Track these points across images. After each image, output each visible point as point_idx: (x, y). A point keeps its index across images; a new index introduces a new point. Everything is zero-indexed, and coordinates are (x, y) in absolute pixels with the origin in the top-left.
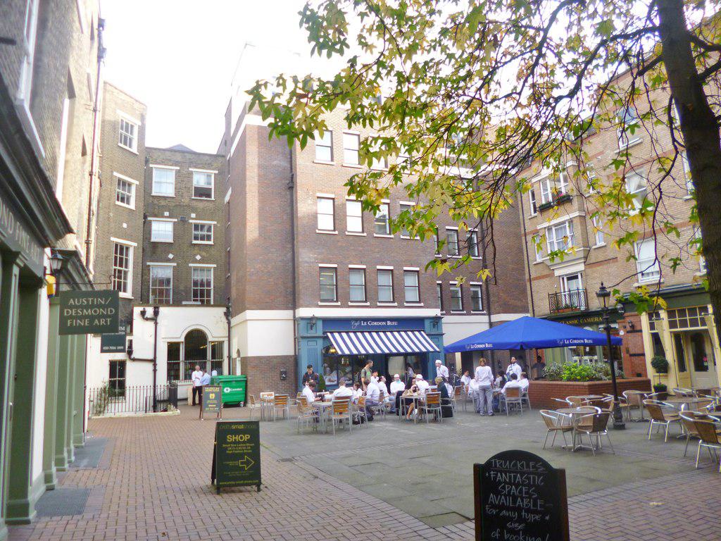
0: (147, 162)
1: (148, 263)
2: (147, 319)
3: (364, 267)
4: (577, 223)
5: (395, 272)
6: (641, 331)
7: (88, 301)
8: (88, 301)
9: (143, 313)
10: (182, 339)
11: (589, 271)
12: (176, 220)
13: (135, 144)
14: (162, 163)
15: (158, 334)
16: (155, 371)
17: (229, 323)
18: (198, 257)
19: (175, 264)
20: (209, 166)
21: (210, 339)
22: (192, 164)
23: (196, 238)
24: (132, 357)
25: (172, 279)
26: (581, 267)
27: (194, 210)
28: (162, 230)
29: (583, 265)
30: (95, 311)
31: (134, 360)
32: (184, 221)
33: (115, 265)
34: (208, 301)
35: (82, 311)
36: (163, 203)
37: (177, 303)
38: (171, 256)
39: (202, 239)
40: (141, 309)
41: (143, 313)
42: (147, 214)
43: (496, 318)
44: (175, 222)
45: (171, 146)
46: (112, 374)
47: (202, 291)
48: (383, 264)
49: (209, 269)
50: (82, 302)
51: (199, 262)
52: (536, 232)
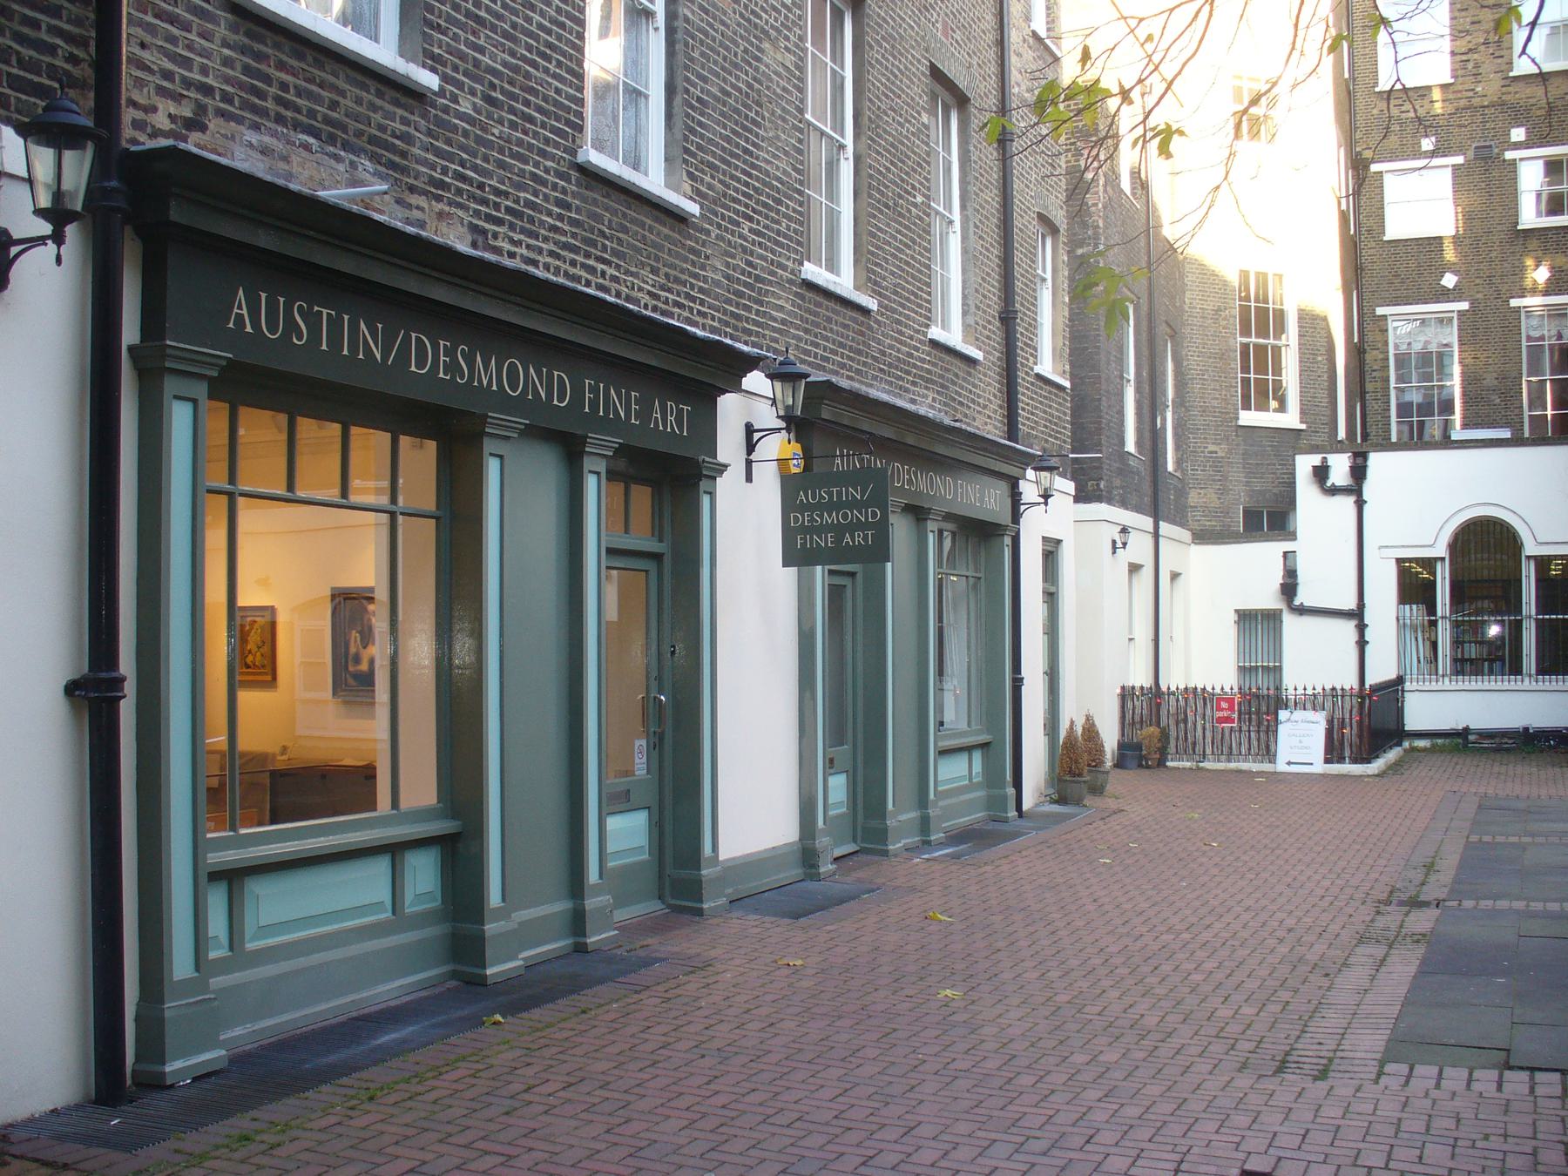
1: (1380, 311)
2: (1334, 491)
7: (830, 494)
8: (830, 494)
9: (1321, 473)
10: (1441, 550)
12: (1460, 160)
16: (1362, 644)
19: (1464, 306)
21: (1530, 549)
24: (1297, 602)
28: (1422, 202)
30: (845, 516)
31: (1302, 611)
33: (1245, 331)
35: (821, 517)
37: (1416, 440)
38: (1449, 280)
40: (1316, 459)
41: (1321, 473)
42: (1368, 154)
44: (1455, 168)
46: (1244, 647)
50: (821, 497)
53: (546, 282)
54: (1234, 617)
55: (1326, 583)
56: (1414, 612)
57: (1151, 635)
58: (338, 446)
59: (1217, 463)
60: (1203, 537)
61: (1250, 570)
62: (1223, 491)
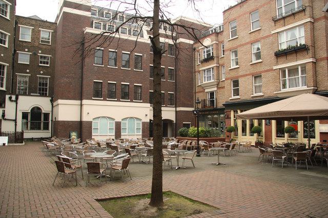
0: (16, 23)
2: (12, 101)
3: (115, 82)
4: (215, 68)
5: (130, 86)
6: (230, 118)
9: (10, 98)
10: (29, 111)
11: (218, 91)
13: (8, 14)
14: (25, 24)
15: (18, 108)
16: (16, 125)
17: (52, 105)
18: (42, 72)
19: (8, 65)
20: (49, 28)
21: (43, 112)
22: (40, 26)
23: (41, 63)
25: (281, 88)
26: (216, 89)
27: (40, 49)
29: (216, 88)
31: (6, 119)
32: (35, 54)
34: (46, 94)
36: (25, 44)
38: (28, 71)
39: (44, 63)
40: (10, 96)
41: (10, 98)
43: (178, 109)
45: (31, 16)
47: (43, 91)
48: (125, 82)
49: (47, 78)
51: (42, 74)
52: (199, 72)
53: (126, 40)
56: (25, 121)
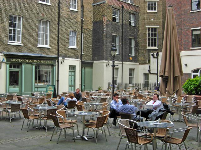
9: (153, 55)
31: (151, 73)
54: (143, 74)
55: (154, 70)
57: (121, 76)
58: (121, 142)
59: (143, 54)
60: (141, 64)
61: (144, 68)
62: (144, 58)
